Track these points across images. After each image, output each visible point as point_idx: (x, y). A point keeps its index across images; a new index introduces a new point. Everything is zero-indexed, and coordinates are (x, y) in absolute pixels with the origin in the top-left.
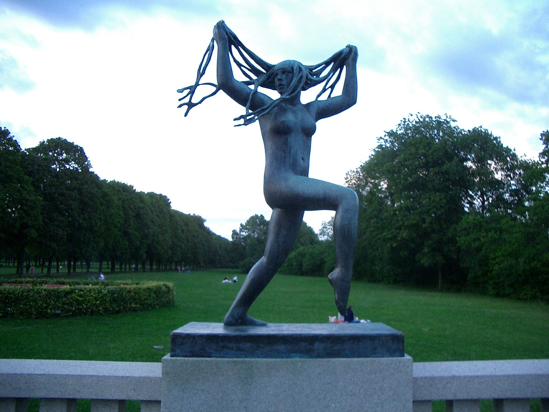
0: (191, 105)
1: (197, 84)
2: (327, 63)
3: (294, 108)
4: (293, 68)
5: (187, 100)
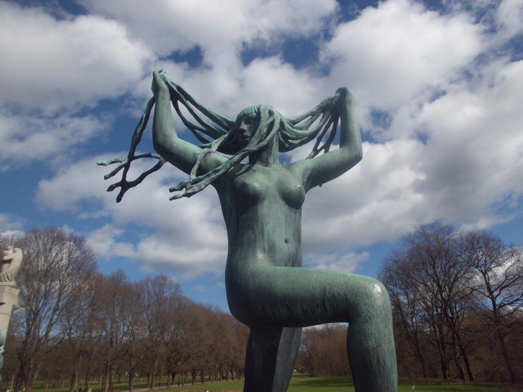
3: (267, 169)
4: (259, 113)
5: (118, 178)
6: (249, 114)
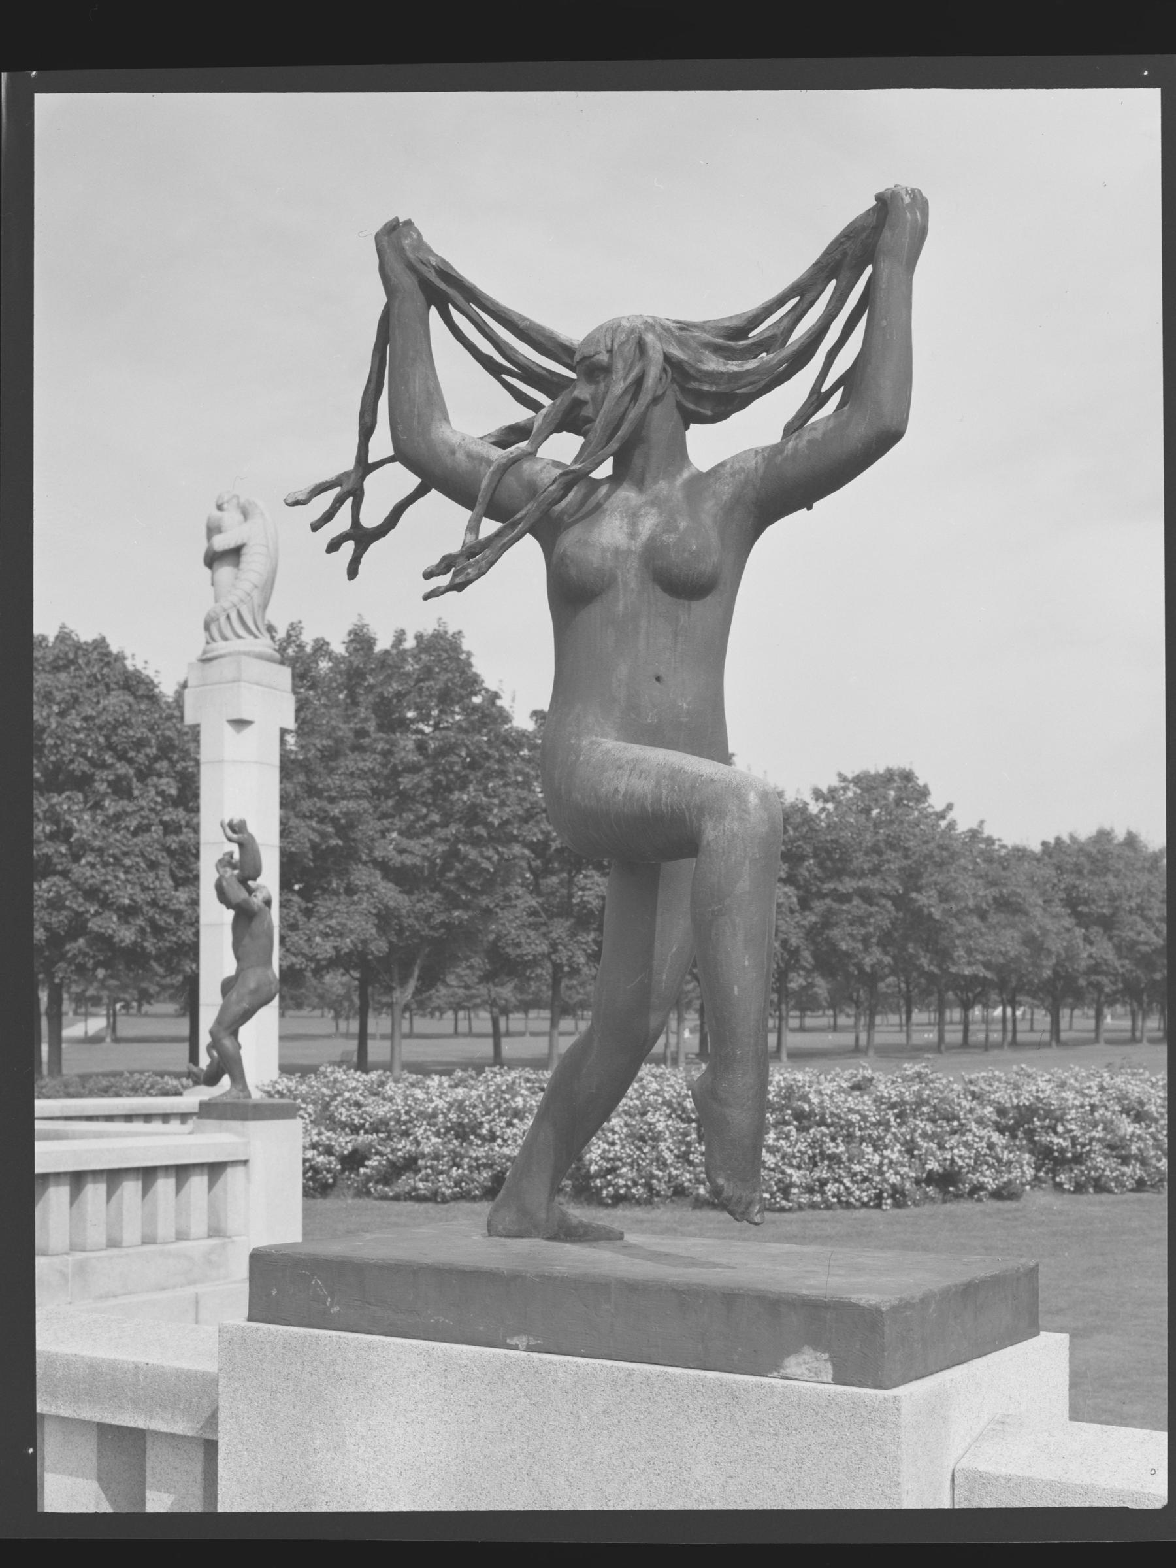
0: (363, 538)
1: (364, 467)
2: (805, 290)
5: (342, 521)
6: (592, 356)
